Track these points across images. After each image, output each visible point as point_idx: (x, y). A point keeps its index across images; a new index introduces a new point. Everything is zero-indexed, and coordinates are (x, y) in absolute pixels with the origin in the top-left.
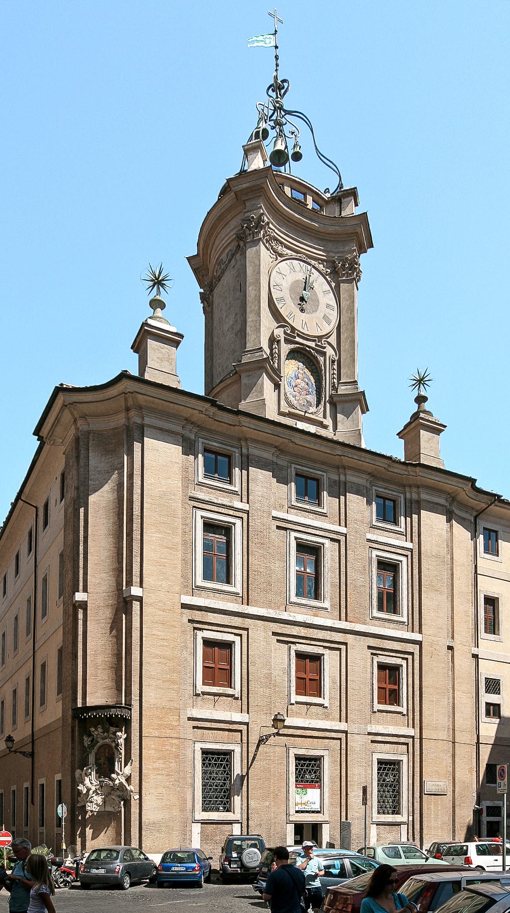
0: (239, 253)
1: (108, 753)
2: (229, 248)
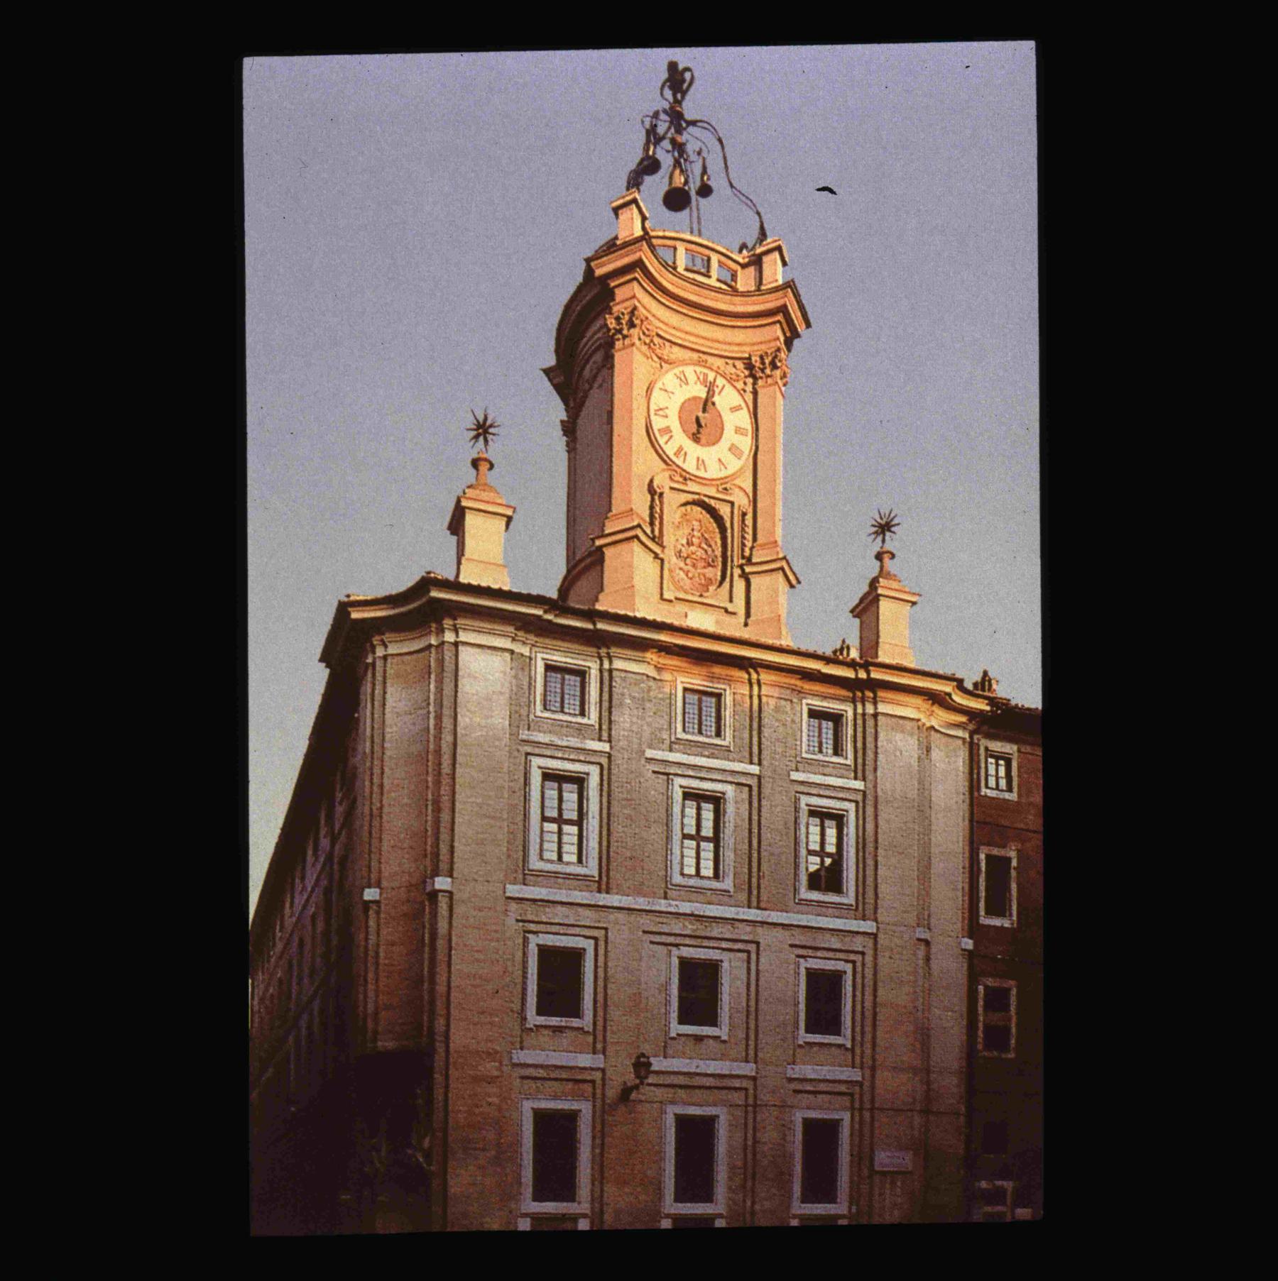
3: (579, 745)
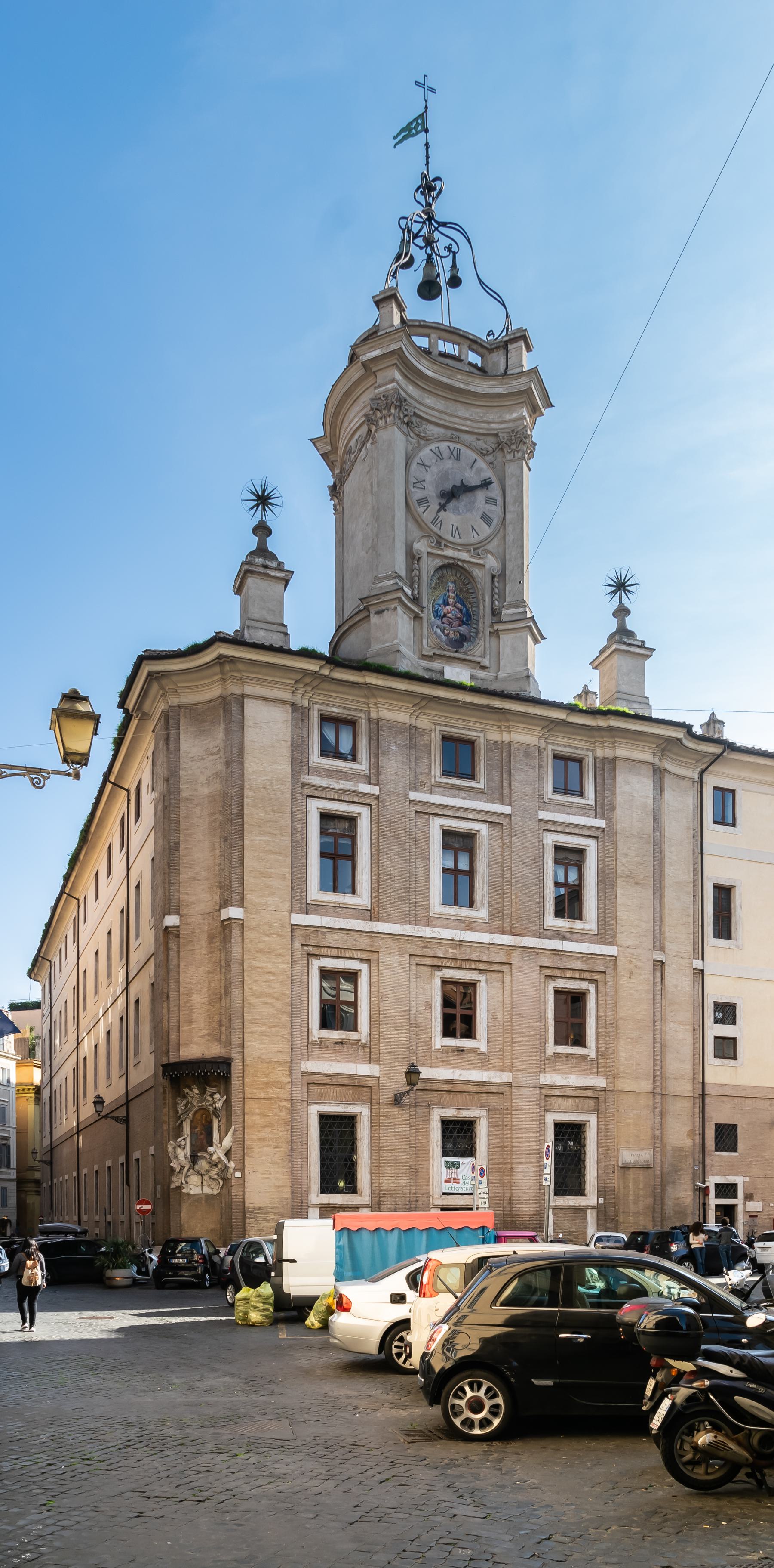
0: (371, 441)
1: (206, 1119)
3: (354, 788)
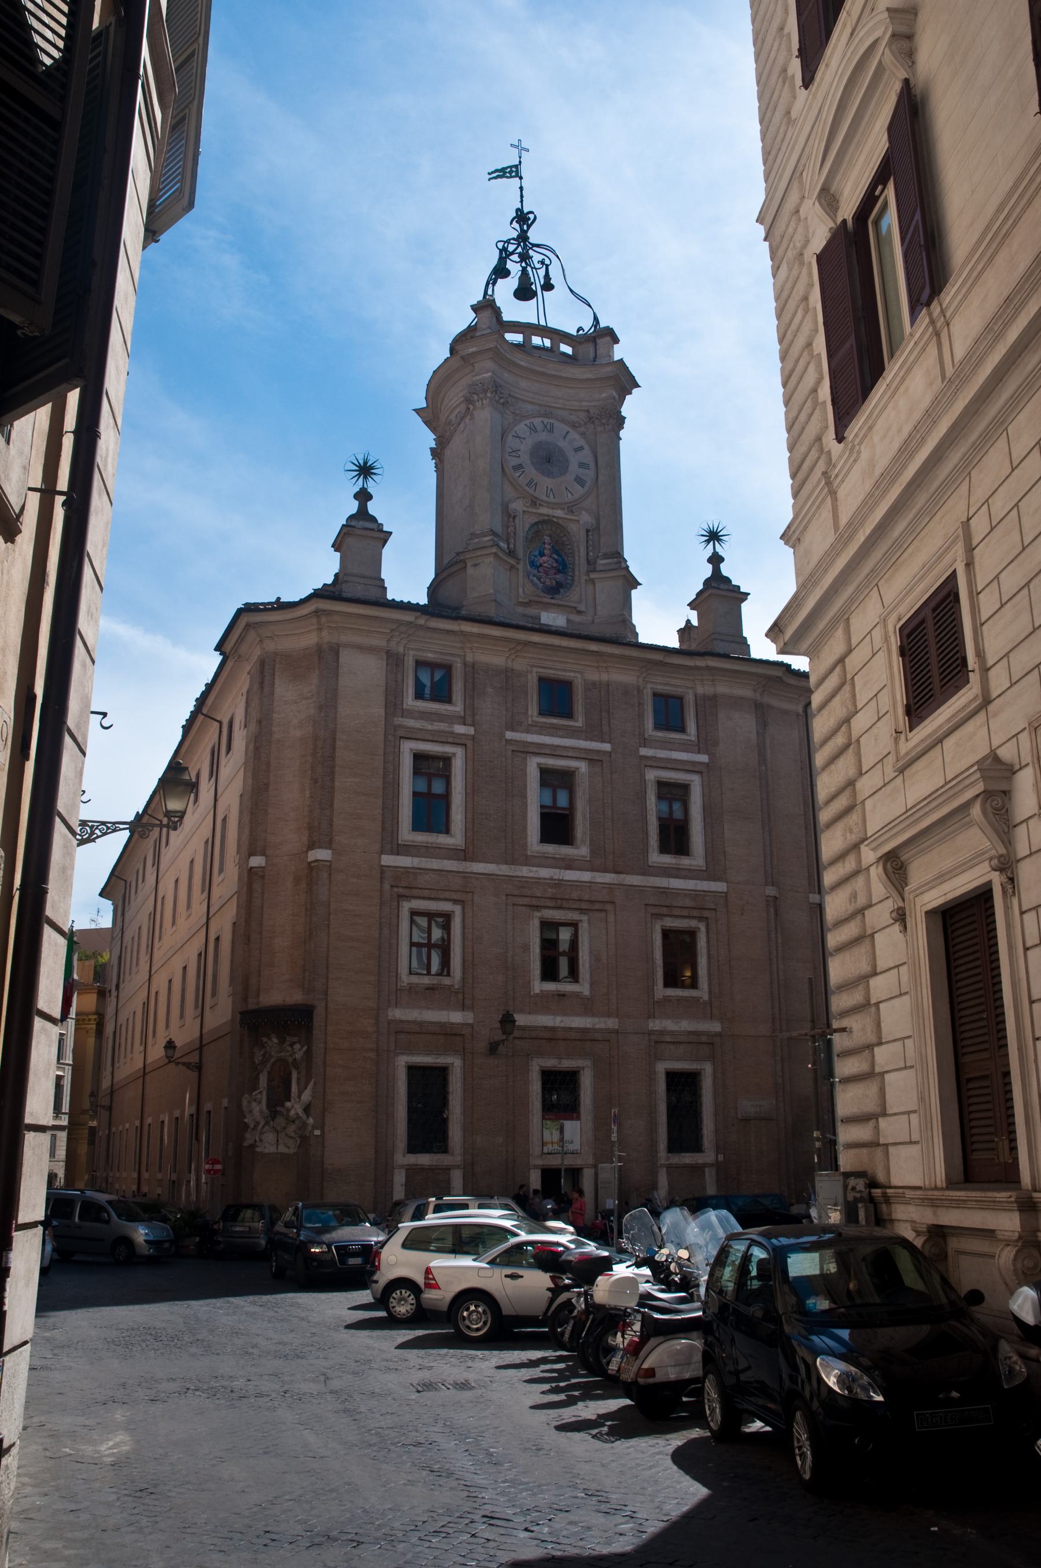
2: (458, 410)
